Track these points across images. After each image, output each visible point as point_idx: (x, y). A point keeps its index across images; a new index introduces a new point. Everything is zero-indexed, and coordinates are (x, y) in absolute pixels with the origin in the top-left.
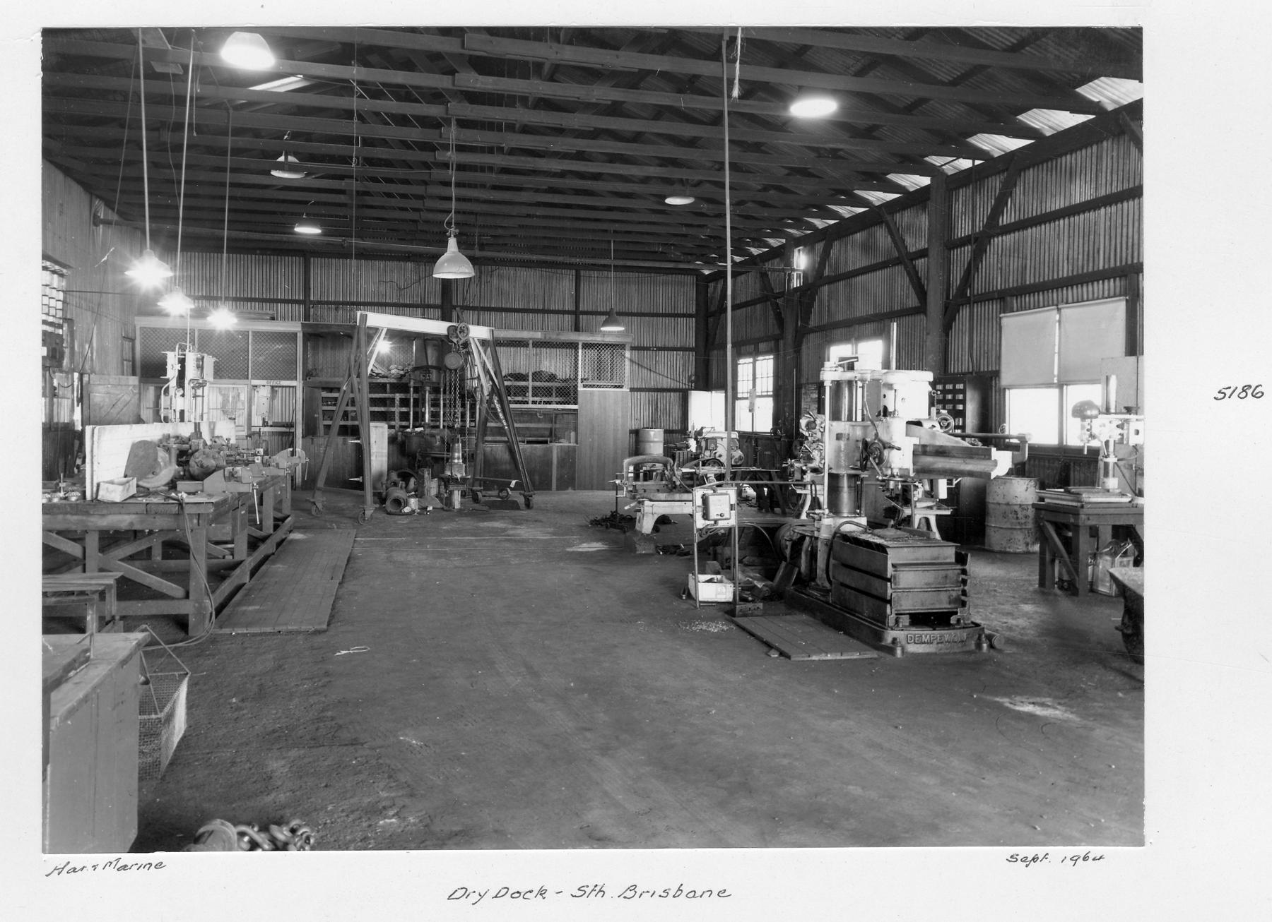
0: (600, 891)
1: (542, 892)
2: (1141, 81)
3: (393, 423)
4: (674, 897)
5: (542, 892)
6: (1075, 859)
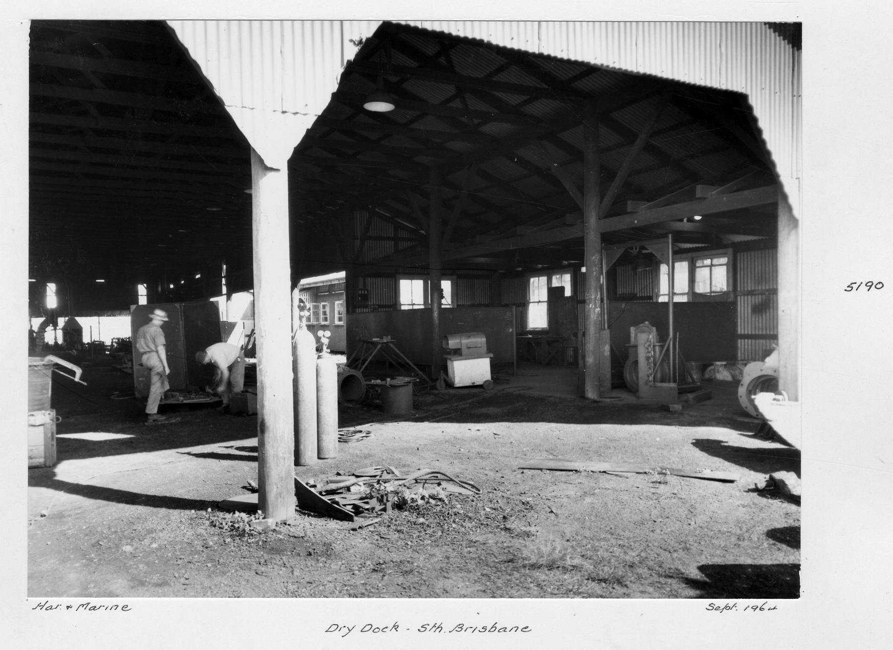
0: (438, 628)
1: (396, 627)
2: (799, 476)
3: (308, 307)
4: (489, 631)
5: (396, 627)
6: (755, 608)
